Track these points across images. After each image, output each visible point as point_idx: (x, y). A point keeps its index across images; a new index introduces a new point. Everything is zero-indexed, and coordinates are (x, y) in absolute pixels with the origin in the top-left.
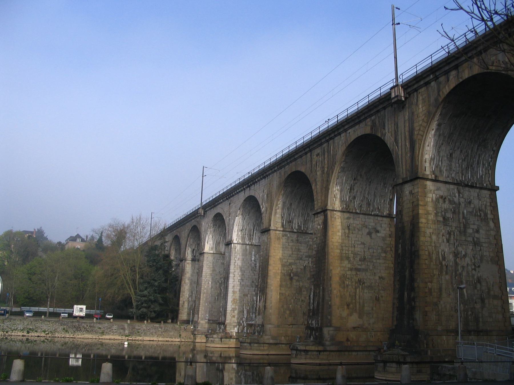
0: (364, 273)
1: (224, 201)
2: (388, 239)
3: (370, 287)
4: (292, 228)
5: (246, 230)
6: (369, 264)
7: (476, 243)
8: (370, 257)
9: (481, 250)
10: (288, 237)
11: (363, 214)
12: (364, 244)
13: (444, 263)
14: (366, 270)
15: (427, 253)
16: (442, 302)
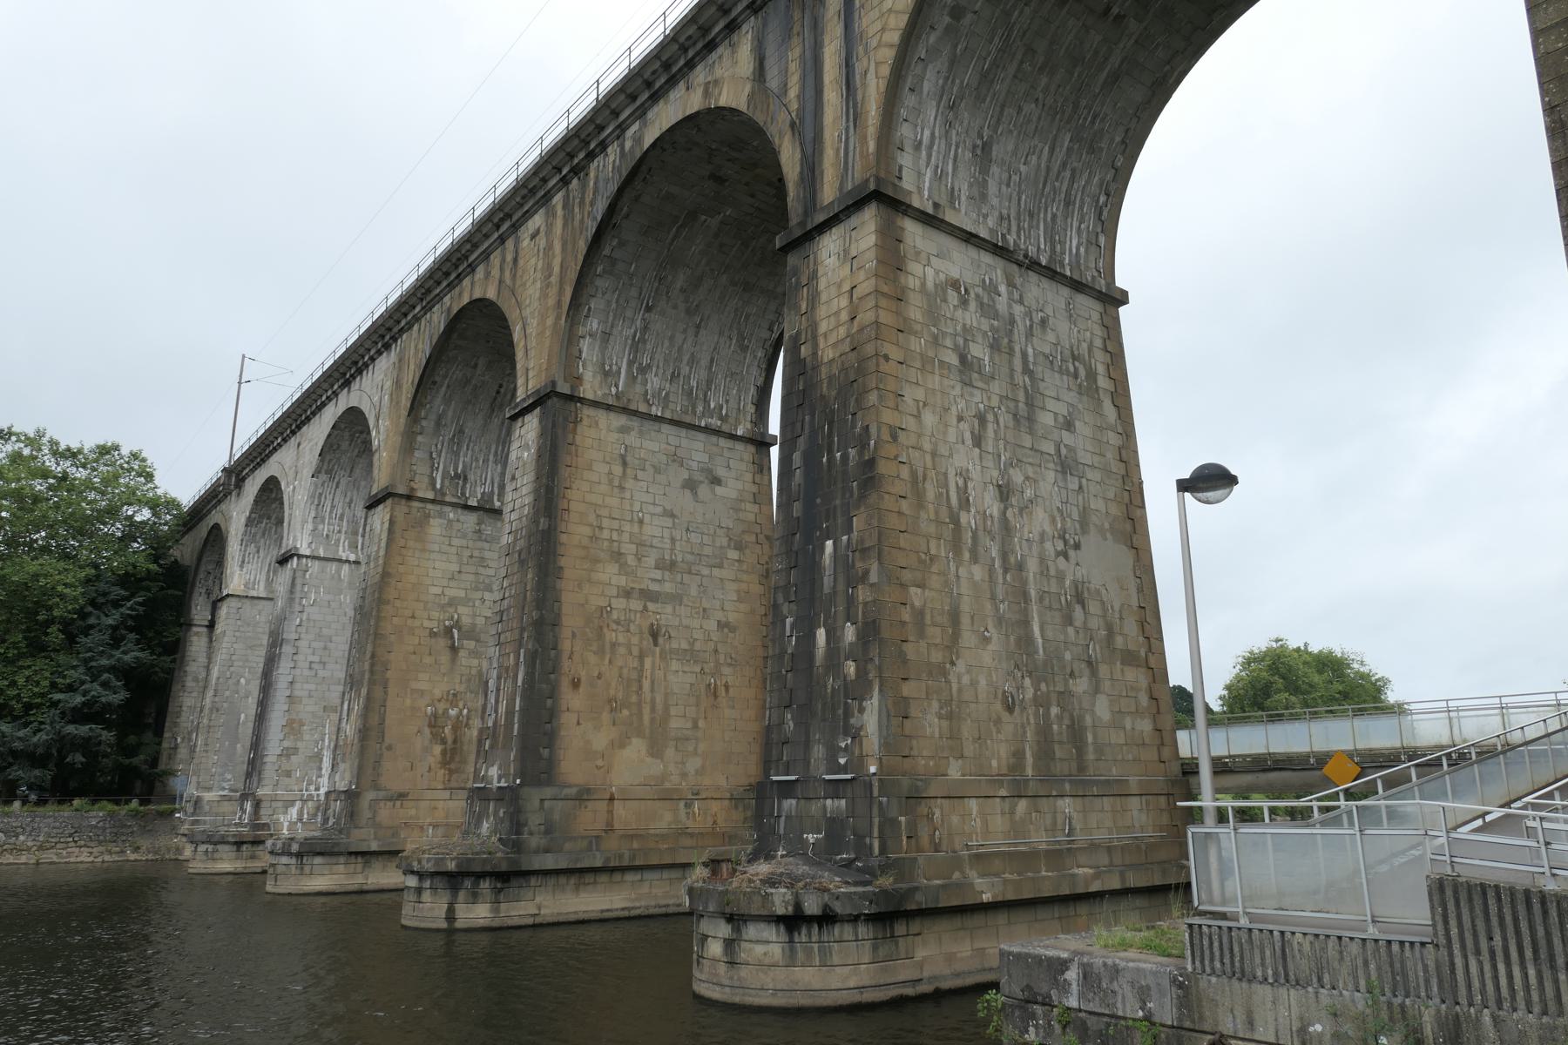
0: (669, 609)
1: (285, 440)
2: (749, 506)
3: (690, 655)
4: (463, 494)
6: (686, 577)
7: (1067, 466)
8: (689, 558)
9: (1080, 487)
11: (673, 422)
12: (673, 516)
13: (964, 518)
14: (676, 599)
15: (905, 472)
16: (961, 667)
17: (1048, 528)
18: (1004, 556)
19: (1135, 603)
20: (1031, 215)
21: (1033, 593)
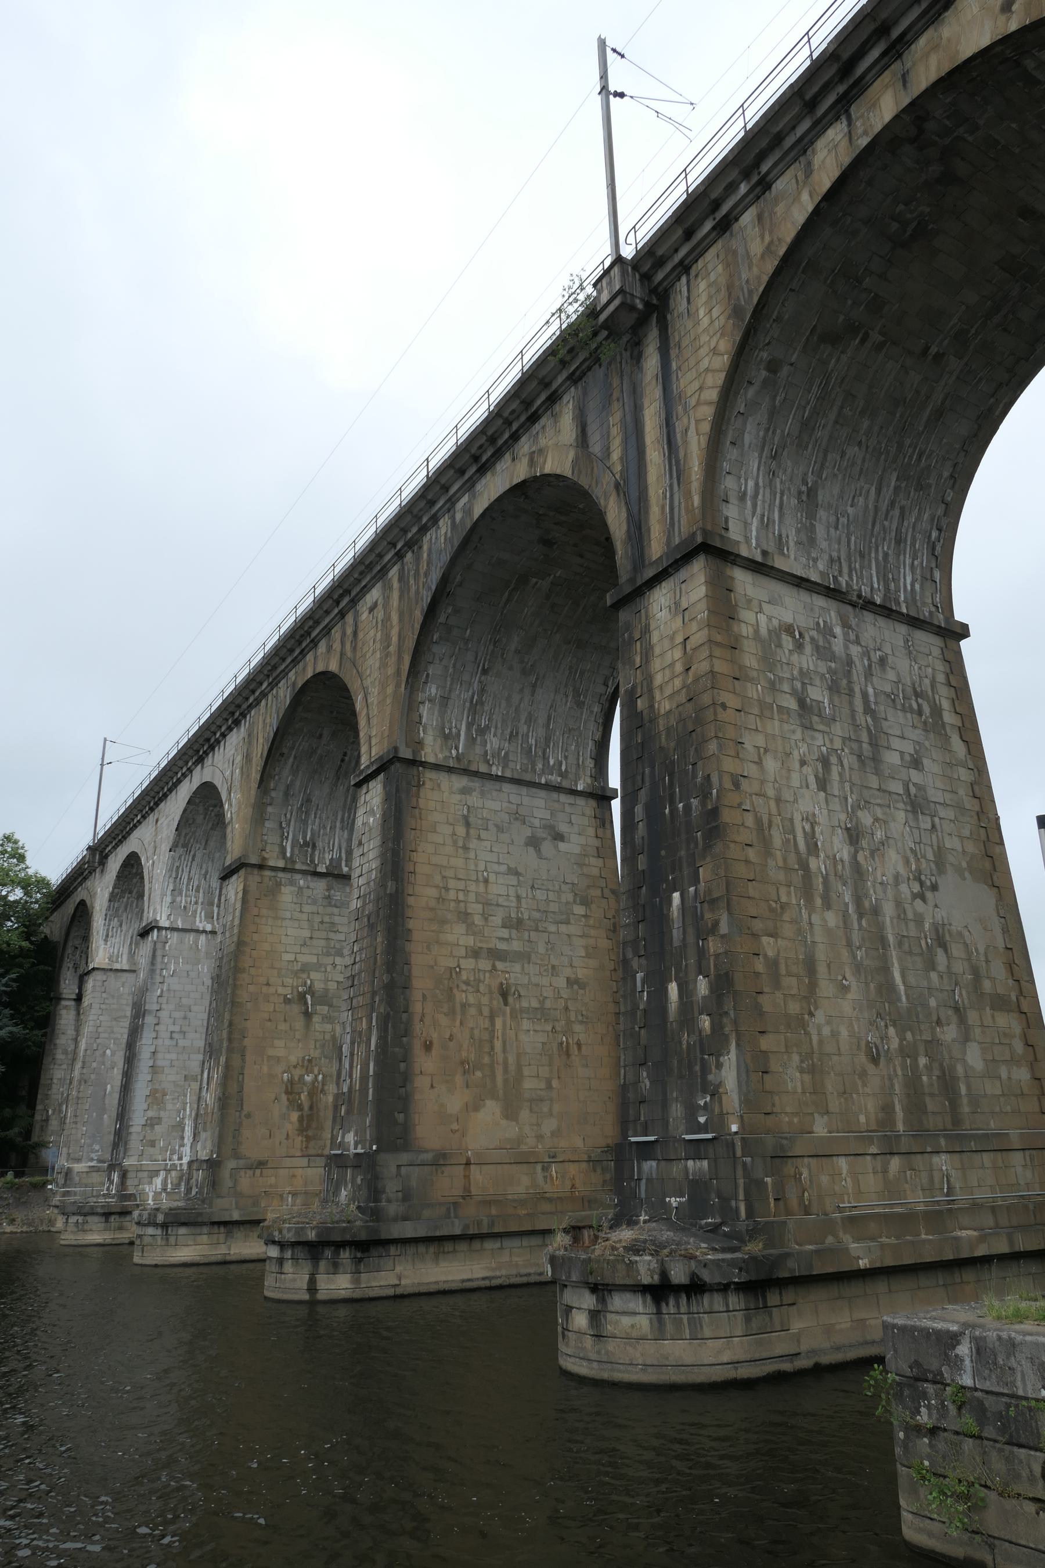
3: (541, 1013)
4: (313, 861)
5: (198, 891)
8: (536, 915)
9: (933, 826)
10: (300, 888)
12: (517, 874)
13: (813, 863)
14: (524, 957)
15: (750, 820)
16: (820, 1017)
17: (902, 870)
18: (858, 900)
19: (1000, 943)
20: (862, 556)
21: (891, 938)
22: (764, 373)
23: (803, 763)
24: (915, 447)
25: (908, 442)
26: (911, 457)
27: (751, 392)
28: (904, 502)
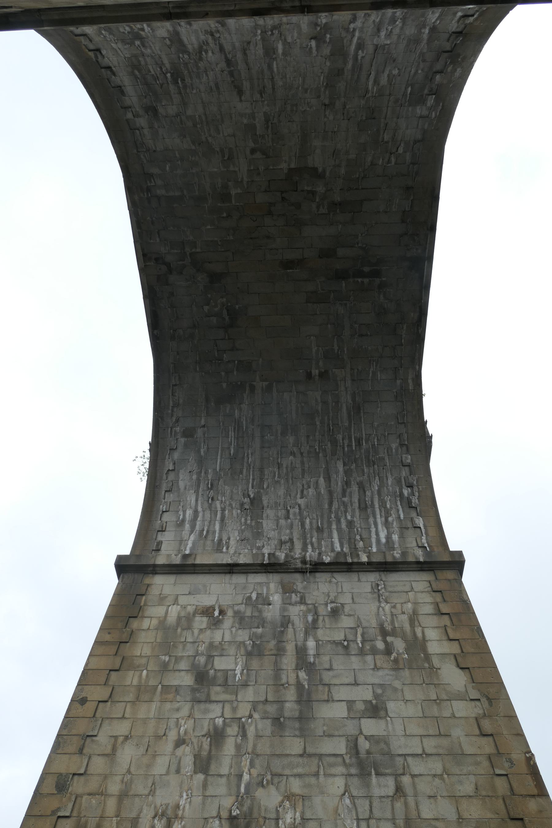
9: (399, 789)
20: (320, 530)
22: (182, 440)
23: (180, 742)
24: (350, 438)
25: (340, 437)
26: (350, 446)
27: (176, 455)
28: (358, 479)
